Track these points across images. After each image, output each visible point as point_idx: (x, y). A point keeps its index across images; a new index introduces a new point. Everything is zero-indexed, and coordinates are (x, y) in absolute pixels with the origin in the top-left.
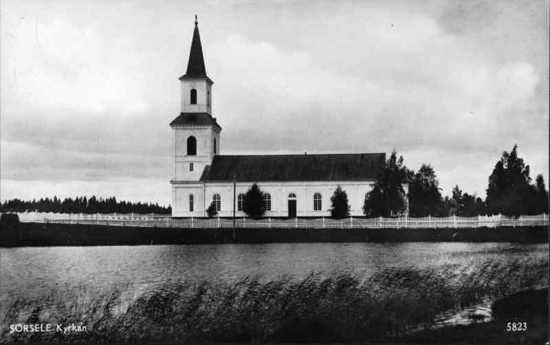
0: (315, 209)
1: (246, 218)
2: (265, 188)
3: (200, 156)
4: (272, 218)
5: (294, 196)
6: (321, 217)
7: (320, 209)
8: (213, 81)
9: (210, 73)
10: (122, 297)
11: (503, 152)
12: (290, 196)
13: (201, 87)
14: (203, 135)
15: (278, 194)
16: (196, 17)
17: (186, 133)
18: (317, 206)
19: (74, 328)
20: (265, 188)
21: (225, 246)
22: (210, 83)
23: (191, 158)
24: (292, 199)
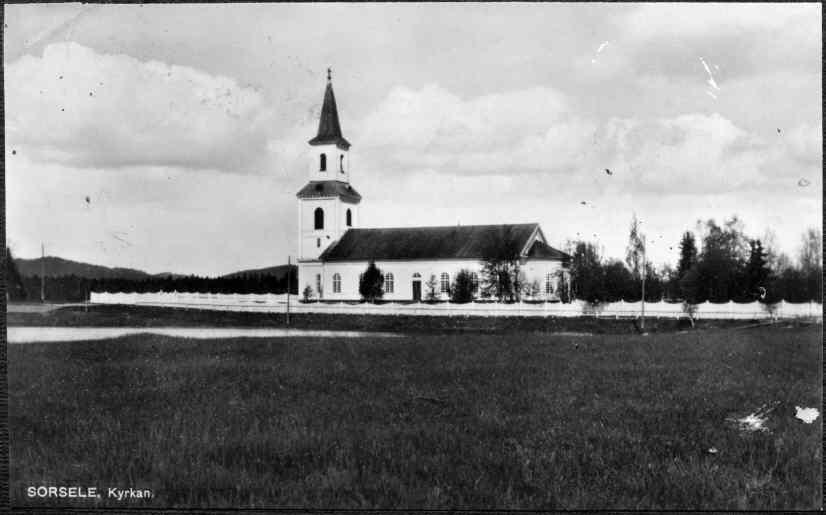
0: (335, 291)
1: (450, 301)
2: (384, 267)
3: (311, 237)
4: (394, 301)
5: (419, 276)
6: (339, 301)
7: (339, 290)
8: (350, 142)
9: (345, 135)
10: (257, 430)
11: (300, 201)
12: (415, 276)
13: (331, 150)
14: (334, 208)
15: (400, 274)
16: (329, 71)
17: (310, 206)
18: (337, 287)
19: (132, 494)
20: (384, 267)
21: (778, 304)
22: (345, 145)
23: (319, 233)
24: (417, 279)
